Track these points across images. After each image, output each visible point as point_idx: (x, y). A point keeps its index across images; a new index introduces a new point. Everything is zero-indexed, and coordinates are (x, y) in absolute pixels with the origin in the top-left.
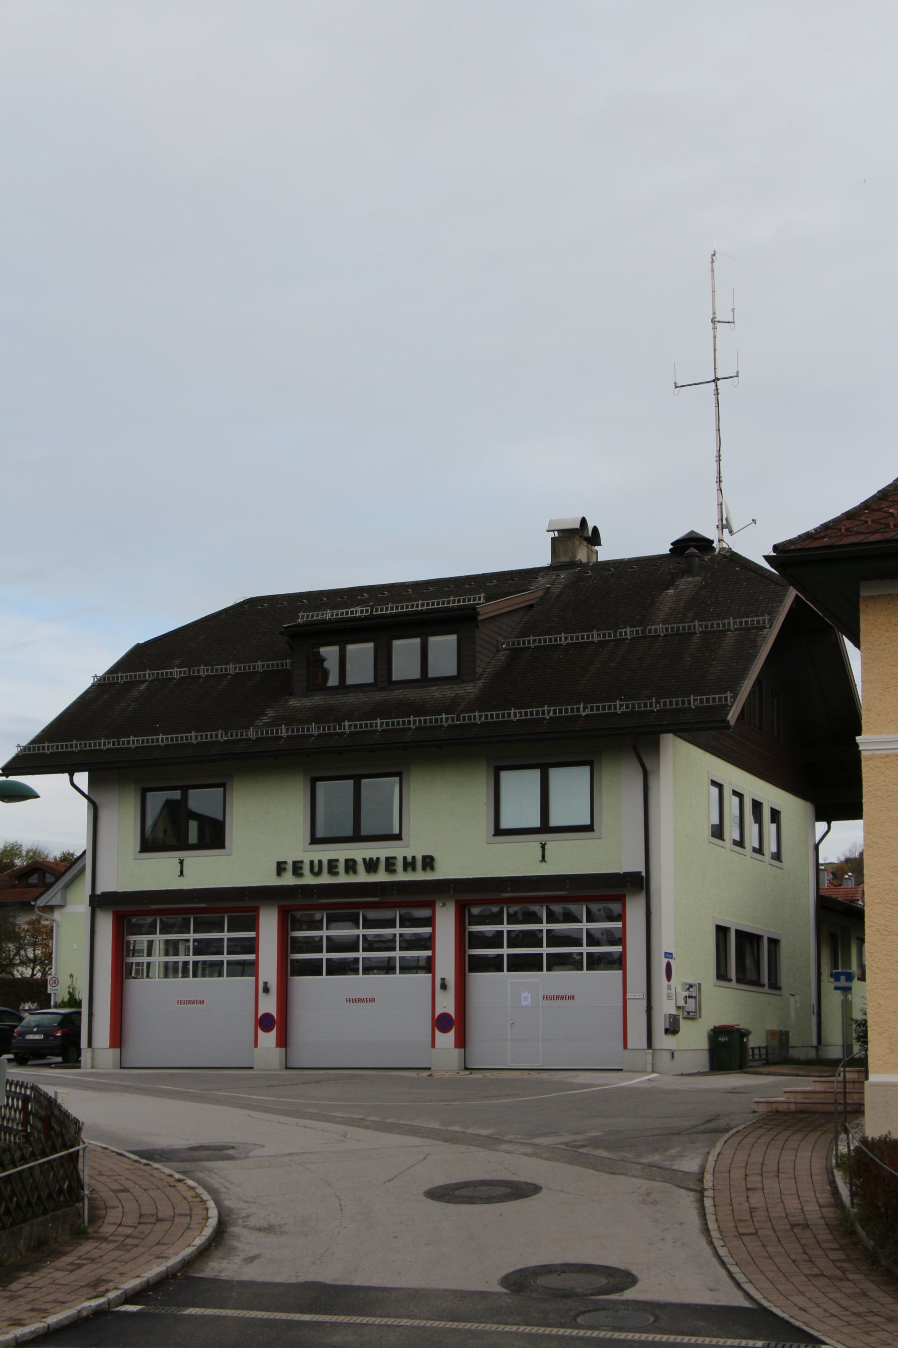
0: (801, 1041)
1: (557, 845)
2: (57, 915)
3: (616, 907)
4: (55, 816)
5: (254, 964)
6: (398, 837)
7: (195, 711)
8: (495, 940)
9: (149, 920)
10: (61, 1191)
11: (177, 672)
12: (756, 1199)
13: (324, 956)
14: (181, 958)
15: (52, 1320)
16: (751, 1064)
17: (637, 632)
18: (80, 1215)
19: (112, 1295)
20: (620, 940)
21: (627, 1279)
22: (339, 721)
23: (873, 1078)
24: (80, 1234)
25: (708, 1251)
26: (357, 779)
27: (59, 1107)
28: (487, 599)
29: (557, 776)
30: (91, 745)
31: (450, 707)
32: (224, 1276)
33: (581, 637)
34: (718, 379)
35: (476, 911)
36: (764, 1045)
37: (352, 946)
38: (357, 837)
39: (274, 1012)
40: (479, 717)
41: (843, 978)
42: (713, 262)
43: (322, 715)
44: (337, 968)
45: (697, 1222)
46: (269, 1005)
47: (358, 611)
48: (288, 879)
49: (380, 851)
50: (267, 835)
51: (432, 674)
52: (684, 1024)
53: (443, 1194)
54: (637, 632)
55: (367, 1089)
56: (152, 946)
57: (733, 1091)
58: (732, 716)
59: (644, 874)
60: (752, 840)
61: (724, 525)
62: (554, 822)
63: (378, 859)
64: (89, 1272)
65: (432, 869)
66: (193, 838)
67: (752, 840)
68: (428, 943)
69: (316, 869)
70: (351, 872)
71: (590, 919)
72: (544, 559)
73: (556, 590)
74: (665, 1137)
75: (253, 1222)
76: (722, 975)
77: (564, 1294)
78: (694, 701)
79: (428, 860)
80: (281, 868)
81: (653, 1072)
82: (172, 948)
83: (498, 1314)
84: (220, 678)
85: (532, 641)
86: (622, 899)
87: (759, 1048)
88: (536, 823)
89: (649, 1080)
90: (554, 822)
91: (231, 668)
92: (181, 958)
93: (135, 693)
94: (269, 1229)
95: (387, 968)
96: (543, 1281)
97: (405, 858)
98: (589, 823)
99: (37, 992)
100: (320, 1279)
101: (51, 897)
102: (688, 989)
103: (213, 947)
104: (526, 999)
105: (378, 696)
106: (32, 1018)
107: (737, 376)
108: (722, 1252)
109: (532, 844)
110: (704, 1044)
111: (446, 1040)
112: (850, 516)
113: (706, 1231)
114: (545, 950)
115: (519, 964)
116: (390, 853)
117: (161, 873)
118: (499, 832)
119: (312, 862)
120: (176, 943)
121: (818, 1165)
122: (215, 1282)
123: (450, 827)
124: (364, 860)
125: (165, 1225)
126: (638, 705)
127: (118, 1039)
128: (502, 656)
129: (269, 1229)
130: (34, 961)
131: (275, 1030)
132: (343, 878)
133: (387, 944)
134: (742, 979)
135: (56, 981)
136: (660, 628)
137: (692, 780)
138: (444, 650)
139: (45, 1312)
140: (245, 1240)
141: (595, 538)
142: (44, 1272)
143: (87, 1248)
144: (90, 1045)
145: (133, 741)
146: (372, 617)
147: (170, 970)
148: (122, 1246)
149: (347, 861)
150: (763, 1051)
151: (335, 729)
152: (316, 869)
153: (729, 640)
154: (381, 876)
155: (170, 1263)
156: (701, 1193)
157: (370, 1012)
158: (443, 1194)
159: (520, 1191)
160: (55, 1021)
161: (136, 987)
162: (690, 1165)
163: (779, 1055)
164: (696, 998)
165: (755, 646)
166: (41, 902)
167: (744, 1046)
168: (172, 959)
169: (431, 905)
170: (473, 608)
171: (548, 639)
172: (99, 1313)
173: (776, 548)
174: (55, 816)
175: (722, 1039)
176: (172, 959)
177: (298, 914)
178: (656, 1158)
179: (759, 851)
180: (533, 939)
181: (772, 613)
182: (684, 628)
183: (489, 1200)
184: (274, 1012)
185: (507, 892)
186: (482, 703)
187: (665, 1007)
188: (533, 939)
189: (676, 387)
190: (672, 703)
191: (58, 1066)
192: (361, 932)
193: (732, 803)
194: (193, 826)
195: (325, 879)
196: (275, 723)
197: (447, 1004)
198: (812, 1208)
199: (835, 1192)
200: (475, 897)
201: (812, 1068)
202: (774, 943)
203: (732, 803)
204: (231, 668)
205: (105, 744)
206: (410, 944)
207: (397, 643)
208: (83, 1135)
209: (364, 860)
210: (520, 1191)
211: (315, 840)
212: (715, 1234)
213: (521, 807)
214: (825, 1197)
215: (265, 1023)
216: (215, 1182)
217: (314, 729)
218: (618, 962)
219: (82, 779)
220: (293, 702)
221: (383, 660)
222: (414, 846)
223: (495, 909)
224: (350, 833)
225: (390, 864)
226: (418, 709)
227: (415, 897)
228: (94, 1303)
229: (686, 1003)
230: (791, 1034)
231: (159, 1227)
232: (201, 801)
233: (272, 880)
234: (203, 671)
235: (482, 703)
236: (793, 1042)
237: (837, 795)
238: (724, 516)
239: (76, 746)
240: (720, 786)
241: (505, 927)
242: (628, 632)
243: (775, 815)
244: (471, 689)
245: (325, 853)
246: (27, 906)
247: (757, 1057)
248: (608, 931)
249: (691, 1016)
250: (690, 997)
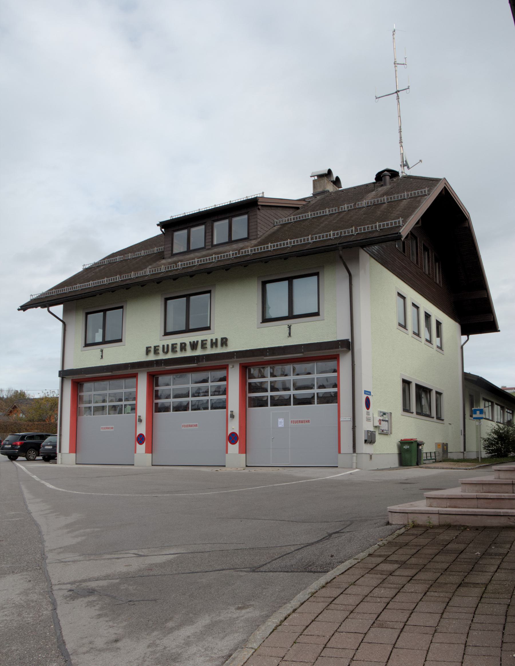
0: (455, 449)
1: (297, 325)
6: (208, 328)
16: (424, 462)
17: (351, 207)
34: (399, 91)
36: (434, 451)
38: (188, 330)
41: (478, 412)
42: (393, 35)
48: (152, 357)
52: (378, 437)
54: (351, 207)
59: (350, 341)
63: (197, 342)
65: (226, 345)
69: (166, 350)
70: (183, 350)
76: (406, 409)
79: (224, 340)
81: (357, 468)
87: (431, 453)
89: (351, 474)
97: (212, 340)
98: (317, 311)
102: (382, 416)
107: (408, 88)
109: (282, 327)
110: (395, 450)
116: (203, 338)
118: (265, 320)
119: (163, 346)
124: (190, 342)
131: (144, 444)
144: (60, 452)
149: (181, 344)
150: (433, 455)
151: (174, 267)
152: (166, 350)
154: (199, 352)
167: (419, 452)
175: (406, 447)
182: (378, 201)
185: (267, 356)
187: (365, 426)
189: (376, 98)
193: (410, 309)
200: (252, 361)
201: (460, 463)
202: (439, 394)
203: (410, 309)
209: (190, 342)
211: (166, 334)
213: (278, 306)
218: (333, 398)
222: (215, 334)
229: (380, 424)
230: (449, 446)
233: (143, 358)
236: (449, 450)
238: (404, 160)
247: (406, 197)
249: (383, 433)
250: (383, 420)
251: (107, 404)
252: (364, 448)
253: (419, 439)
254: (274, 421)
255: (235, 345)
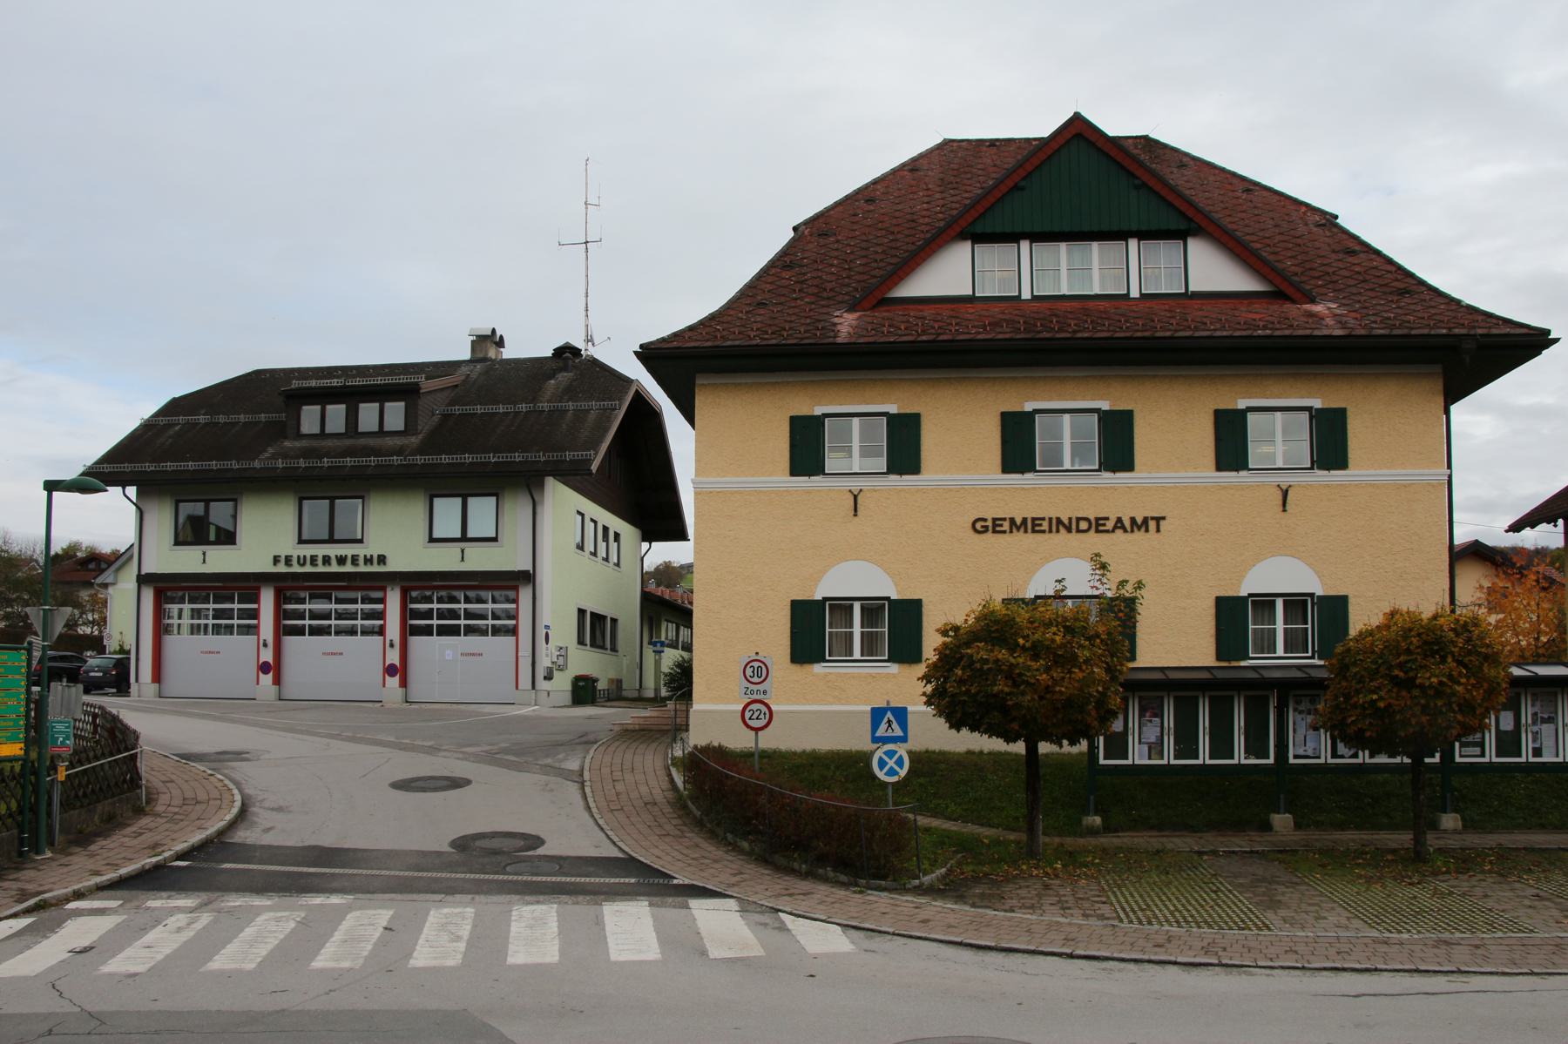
0: (630, 687)
2: (111, 590)
3: (512, 594)
4: (107, 522)
5: (257, 627)
6: (361, 541)
7: (202, 450)
8: (428, 615)
9: (180, 594)
10: (125, 781)
11: (202, 419)
12: (620, 787)
13: (307, 622)
14: (203, 622)
15: (123, 871)
18: (139, 798)
19: (166, 854)
20: (515, 617)
21: (538, 841)
22: (320, 457)
23: (698, 706)
24: (139, 812)
25: (591, 821)
26: (332, 499)
27: (121, 722)
28: (427, 378)
29: (473, 502)
30: (139, 467)
31: (399, 451)
32: (249, 841)
33: (491, 408)
35: (414, 594)
37: (327, 616)
38: (331, 540)
39: (270, 660)
40: (420, 460)
43: (307, 453)
44: (315, 631)
45: (581, 803)
46: (267, 656)
47: (335, 382)
48: (282, 568)
49: (347, 550)
50: (266, 536)
51: (386, 429)
53: (403, 785)
55: (340, 713)
56: (181, 613)
57: (590, 718)
58: (594, 467)
60: (602, 552)
61: (589, 340)
62: (470, 534)
64: (148, 838)
66: (212, 537)
67: (602, 552)
68: (381, 615)
71: (494, 601)
72: (467, 356)
73: (474, 376)
74: (557, 746)
75: (267, 804)
76: (581, 642)
77: (495, 852)
78: (569, 455)
80: (276, 560)
82: (196, 614)
83: (450, 866)
84: (233, 424)
85: (457, 410)
86: (516, 588)
88: (458, 535)
90: (470, 534)
91: (242, 418)
92: (203, 622)
93: (171, 432)
94: (280, 809)
95: (352, 632)
96: (478, 843)
99: (97, 644)
100: (320, 843)
101: (107, 577)
103: (228, 614)
104: (449, 655)
105: (348, 442)
106: (93, 661)
108: (601, 822)
109: (455, 549)
111: (393, 682)
112: (691, 328)
113: (588, 808)
114: (462, 622)
115: (444, 631)
117: (189, 560)
118: (432, 540)
120: (199, 610)
121: (659, 763)
122: (243, 846)
123: (397, 534)
125: (203, 806)
126: (530, 456)
127: (157, 676)
128: (436, 419)
129: (280, 809)
130: (93, 623)
132: (321, 569)
133: (352, 616)
134: (593, 645)
135: (110, 637)
136: (545, 406)
137: (565, 509)
138: (395, 414)
139: (117, 866)
140: (262, 817)
141: (500, 343)
142: (114, 838)
143: (145, 821)
145: (170, 466)
146: (345, 387)
147: (195, 630)
148: (172, 820)
153: (592, 416)
155: (209, 832)
156: (582, 784)
157: (340, 662)
158: (403, 785)
159: (456, 783)
160: (110, 663)
161: (170, 641)
162: (573, 765)
163: (616, 695)
164: (565, 656)
165: (609, 420)
166: (99, 580)
168: (196, 622)
169: (384, 589)
170: (417, 384)
171: (468, 409)
172: (157, 867)
173: (641, 346)
174: (107, 522)
176: (196, 622)
177: (288, 594)
178: (549, 761)
179: (606, 559)
180: (454, 614)
181: (621, 399)
183: (436, 790)
184: (270, 660)
186: (421, 450)
187: (544, 662)
188: (454, 614)
190: (553, 456)
191: (113, 695)
192: (333, 606)
193: (590, 527)
194: (212, 531)
195: (308, 569)
196: (274, 457)
197: (394, 657)
198: (659, 796)
199: (672, 781)
200: (414, 583)
202: (614, 621)
203: (590, 527)
204: (242, 418)
205: (150, 467)
206: (368, 616)
207: (362, 406)
208: (141, 741)
210: (456, 783)
211: (301, 541)
212: (594, 810)
214: (666, 785)
215: (264, 668)
216: (237, 776)
217: (302, 463)
218: (514, 631)
219: (132, 491)
220: (287, 444)
221: (352, 418)
223: (428, 593)
224: (326, 537)
225: (355, 560)
226: (376, 452)
227: (372, 583)
228: (154, 860)
231: (198, 807)
232: (219, 513)
233: (269, 568)
234: (222, 419)
235: (421, 450)
237: (661, 520)
239: (127, 467)
240: (582, 515)
241: (435, 606)
242: (523, 407)
243: (617, 536)
244: (414, 440)
245: (308, 551)
246: (90, 585)
248: (506, 610)
249: (560, 669)
251: (211, 622)
252: (542, 685)
253: (594, 675)
254: (435, 655)
255: (395, 565)
